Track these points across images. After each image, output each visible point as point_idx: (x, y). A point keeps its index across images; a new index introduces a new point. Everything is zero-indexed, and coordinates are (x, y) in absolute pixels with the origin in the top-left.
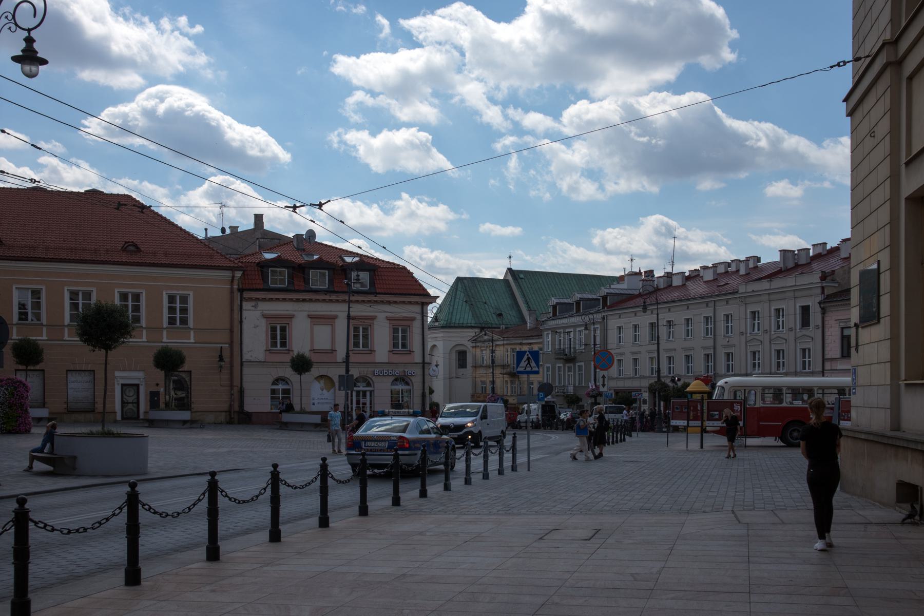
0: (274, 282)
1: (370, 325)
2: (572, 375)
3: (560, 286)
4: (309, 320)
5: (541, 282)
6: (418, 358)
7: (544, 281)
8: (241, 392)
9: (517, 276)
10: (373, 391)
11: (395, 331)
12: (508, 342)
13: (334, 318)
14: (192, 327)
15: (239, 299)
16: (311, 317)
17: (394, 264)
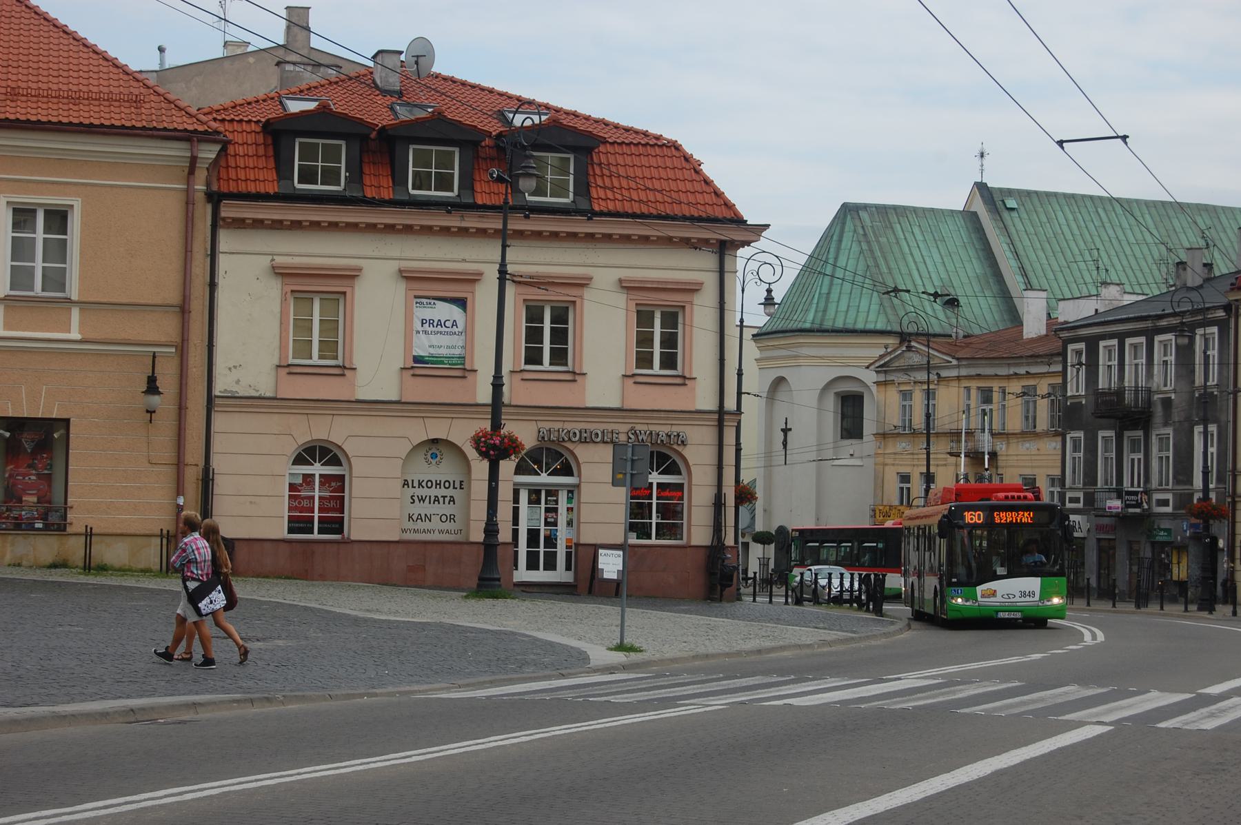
0: (309, 175)
1: (574, 302)
2: (1139, 460)
3: (1111, 232)
4: (402, 286)
5: (1062, 221)
6: (705, 399)
7: (1070, 217)
8: (207, 480)
9: (999, 204)
10: (578, 486)
11: (644, 318)
12: (973, 371)
13: (472, 279)
14: (75, 297)
15: (209, 222)
16: (409, 277)
17: (646, 134)
